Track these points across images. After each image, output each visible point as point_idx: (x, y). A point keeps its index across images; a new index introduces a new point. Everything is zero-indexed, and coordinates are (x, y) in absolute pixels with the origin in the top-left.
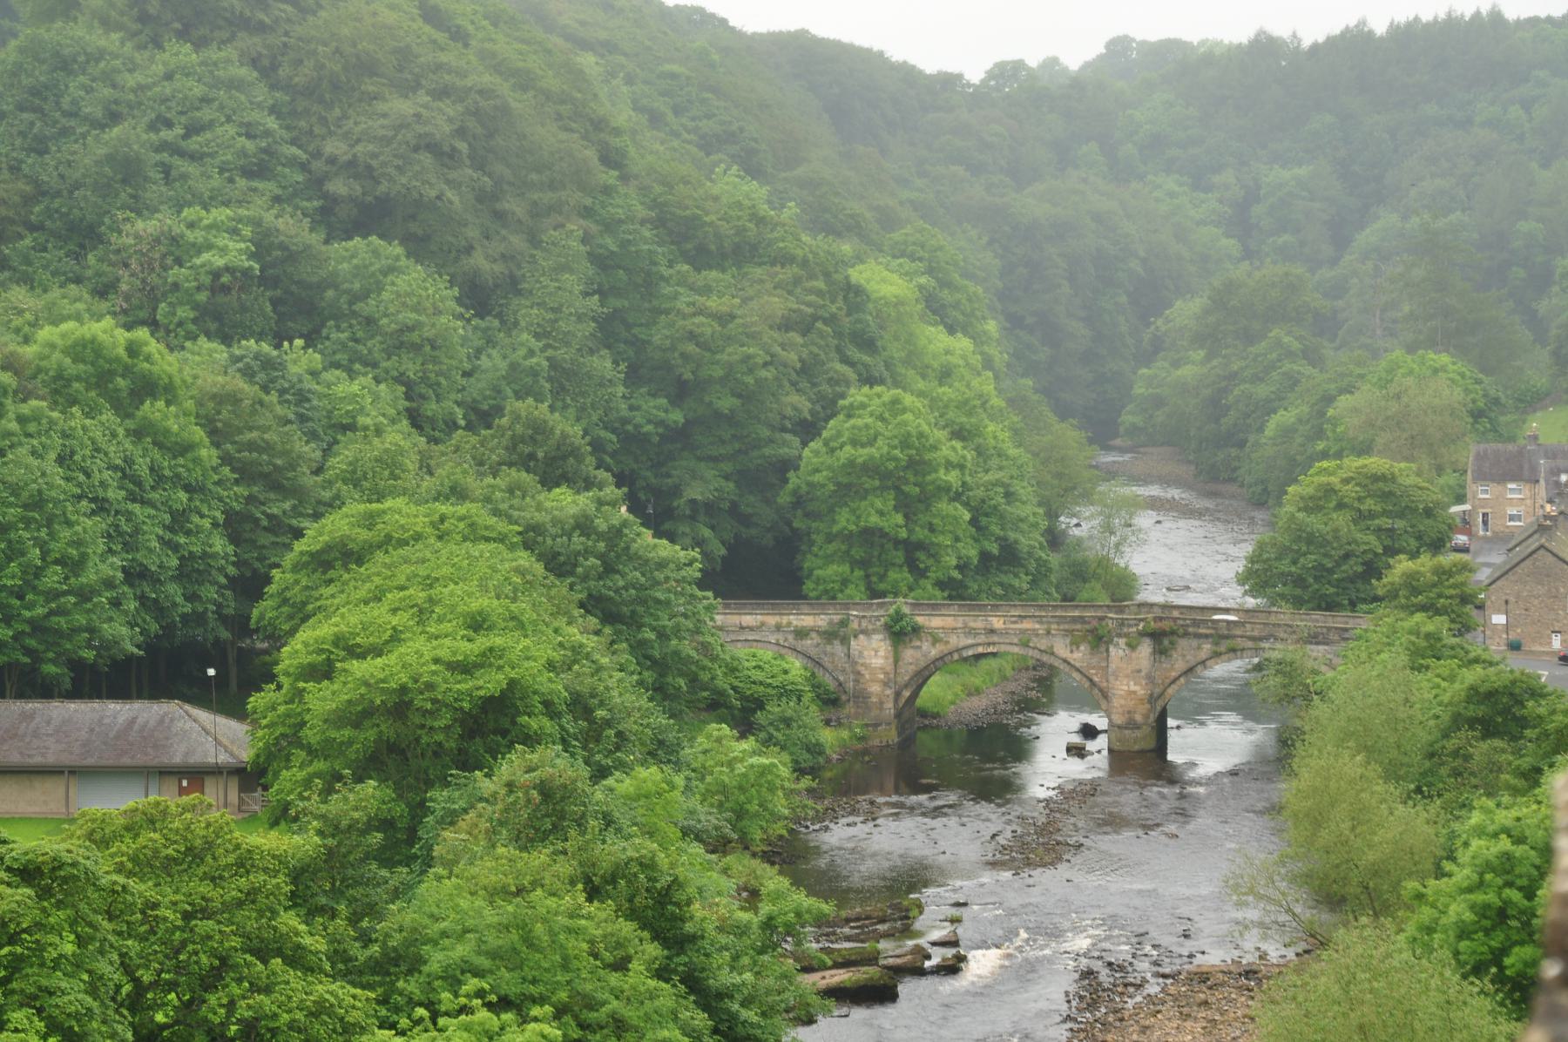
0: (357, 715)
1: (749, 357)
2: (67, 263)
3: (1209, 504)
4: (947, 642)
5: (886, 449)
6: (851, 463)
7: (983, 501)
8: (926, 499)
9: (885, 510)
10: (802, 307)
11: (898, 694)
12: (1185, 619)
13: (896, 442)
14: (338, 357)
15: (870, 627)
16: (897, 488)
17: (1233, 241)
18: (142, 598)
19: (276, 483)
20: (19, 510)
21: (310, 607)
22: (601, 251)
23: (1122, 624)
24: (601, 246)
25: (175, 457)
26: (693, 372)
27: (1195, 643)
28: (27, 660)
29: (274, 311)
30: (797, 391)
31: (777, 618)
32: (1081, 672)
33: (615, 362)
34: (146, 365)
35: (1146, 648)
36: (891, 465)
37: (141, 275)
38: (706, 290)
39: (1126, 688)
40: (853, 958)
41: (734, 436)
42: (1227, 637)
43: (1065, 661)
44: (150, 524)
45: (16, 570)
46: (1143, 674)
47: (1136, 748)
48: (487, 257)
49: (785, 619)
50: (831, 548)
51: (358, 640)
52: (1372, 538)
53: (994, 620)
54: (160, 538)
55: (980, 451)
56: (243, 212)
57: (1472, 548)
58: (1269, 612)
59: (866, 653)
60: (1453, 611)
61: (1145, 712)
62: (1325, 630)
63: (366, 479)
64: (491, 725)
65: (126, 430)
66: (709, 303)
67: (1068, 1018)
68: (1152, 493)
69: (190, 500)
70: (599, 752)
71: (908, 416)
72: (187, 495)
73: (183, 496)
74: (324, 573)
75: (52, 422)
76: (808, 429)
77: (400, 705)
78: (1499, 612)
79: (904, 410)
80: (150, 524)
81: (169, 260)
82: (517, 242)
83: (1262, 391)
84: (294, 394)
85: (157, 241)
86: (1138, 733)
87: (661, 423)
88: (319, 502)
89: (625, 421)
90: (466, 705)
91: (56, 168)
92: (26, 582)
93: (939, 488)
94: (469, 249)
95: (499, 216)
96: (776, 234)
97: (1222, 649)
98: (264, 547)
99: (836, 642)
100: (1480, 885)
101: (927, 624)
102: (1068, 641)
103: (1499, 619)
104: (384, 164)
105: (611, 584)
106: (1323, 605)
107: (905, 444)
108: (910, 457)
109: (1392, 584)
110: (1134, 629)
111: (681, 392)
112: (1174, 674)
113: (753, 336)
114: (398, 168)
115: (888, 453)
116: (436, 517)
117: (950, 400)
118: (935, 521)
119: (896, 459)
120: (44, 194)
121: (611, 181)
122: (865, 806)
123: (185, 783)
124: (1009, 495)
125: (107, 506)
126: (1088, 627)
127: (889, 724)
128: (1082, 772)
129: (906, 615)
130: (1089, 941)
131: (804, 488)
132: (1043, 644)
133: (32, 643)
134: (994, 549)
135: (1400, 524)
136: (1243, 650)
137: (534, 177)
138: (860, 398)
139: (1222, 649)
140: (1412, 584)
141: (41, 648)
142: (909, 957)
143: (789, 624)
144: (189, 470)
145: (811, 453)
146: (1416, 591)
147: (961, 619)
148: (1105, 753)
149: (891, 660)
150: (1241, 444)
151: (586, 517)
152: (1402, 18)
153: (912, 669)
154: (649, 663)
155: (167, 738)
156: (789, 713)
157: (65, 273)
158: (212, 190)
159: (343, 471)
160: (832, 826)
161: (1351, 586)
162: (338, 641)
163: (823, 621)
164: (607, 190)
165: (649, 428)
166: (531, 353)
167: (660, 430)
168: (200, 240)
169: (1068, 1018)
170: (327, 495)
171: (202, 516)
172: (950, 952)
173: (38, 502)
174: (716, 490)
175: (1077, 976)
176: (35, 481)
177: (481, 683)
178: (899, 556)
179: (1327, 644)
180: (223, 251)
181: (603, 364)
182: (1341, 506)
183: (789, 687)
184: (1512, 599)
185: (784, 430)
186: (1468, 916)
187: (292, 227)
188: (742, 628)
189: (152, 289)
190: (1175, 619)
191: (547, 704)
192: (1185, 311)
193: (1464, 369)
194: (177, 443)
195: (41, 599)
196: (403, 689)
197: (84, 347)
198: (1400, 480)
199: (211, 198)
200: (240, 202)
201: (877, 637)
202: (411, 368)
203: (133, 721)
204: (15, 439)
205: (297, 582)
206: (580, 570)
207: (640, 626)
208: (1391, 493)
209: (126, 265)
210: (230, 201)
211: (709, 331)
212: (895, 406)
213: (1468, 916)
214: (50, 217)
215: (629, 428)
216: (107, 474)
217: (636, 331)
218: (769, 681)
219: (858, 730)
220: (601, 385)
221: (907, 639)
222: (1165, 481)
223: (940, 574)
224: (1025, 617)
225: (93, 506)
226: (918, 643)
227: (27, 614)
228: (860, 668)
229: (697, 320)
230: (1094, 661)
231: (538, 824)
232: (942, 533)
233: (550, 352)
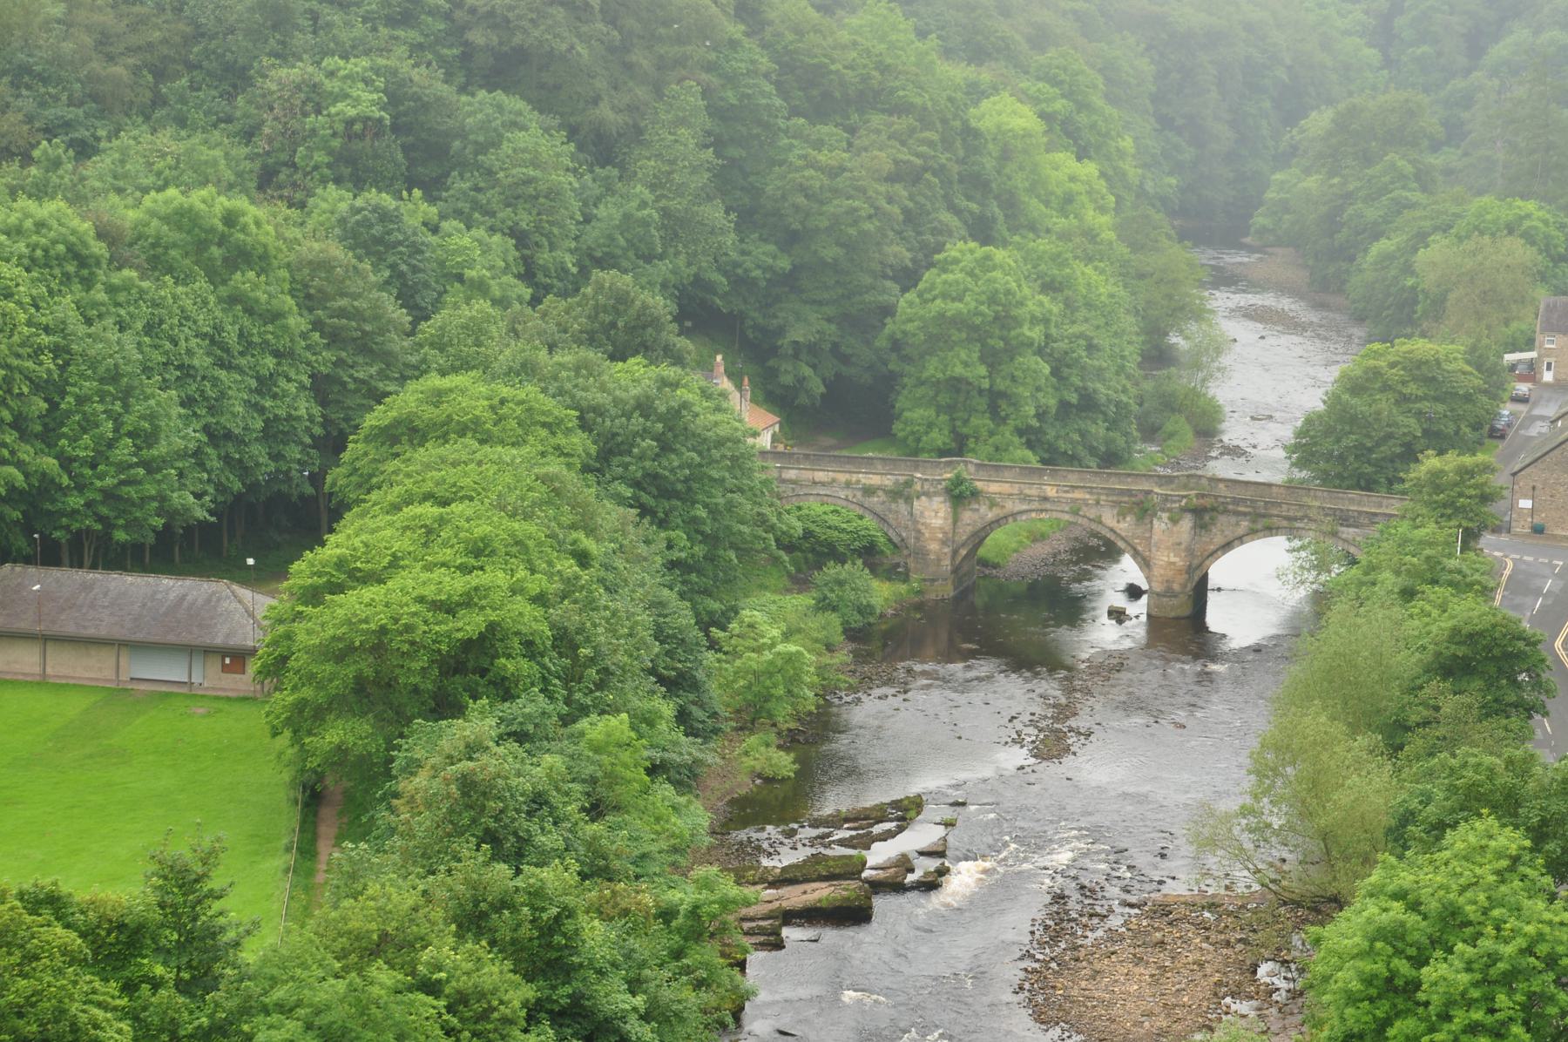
0: (340, 652)
1: (856, 210)
2: (219, 103)
3: (1313, 317)
4: (1003, 507)
5: (973, 304)
6: (941, 315)
7: (1066, 353)
8: (1012, 351)
10: (912, 158)
11: (955, 552)
13: (984, 297)
14: (460, 205)
15: (932, 490)
17: (1373, 51)
18: (227, 459)
19: (366, 347)
20: (95, 384)
21: (374, 480)
22: (722, 104)
23: (1166, 500)
24: (722, 99)
25: (265, 324)
27: (1233, 519)
28: (99, 527)
29: (406, 156)
30: (902, 239)
31: (847, 476)
32: (1126, 541)
33: (727, 212)
34: (241, 236)
35: (1187, 523)
36: (978, 320)
37: (283, 120)
38: (818, 145)
40: (837, 871)
41: (837, 282)
42: (1264, 516)
43: (1112, 530)
44: (236, 390)
45: (89, 442)
46: (1183, 547)
47: (1173, 614)
48: (613, 108)
49: (854, 478)
50: (920, 391)
51: (358, 564)
52: (1412, 421)
53: (1048, 488)
54: (247, 403)
55: (1068, 304)
56: (381, 61)
57: (1532, 400)
59: (926, 513)
60: (1472, 510)
63: (452, 345)
64: (471, 665)
65: (218, 297)
66: (821, 157)
67: (1029, 955)
68: (1267, 303)
69: (279, 364)
70: (580, 690)
71: (997, 274)
72: (274, 361)
73: (270, 362)
74: (392, 446)
75: (142, 292)
76: (908, 278)
77: (379, 645)
78: (1525, 497)
79: (994, 268)
80: (236, 390)
81: (309, 108)
82: (642, 93)
83: (1372, 214)
84: (407, 246)
85: (298, 88)
86: (1175, 601)
87: (771, 268)
88: (406, 365)
89: (736, 265)
90: (444, 648)
91: (213, 11)
92: (98, 452)
93: (1023, 344)
94: (596, 101)
95: (629, 67)
96: (897, 83)
97: (1259, 526)
98: (349, 408)
99: (901, 501)
100: (1368, 953)
101: (985, 488)
102: (1115, 512)
103: (1526, 504)
104: (520, 17)
105: (666, 464)
106: (1363, 483)
108: (997, 312)
109: (1419, 479)
111: (790, 239)
112: (1212, 547)
113: (863, 191)
114: (532, 20)
116: (496, 401)
117: (1045, 252)
118: (1016, 373)
120: (202, 35)
121: (738, 36)
122: (901, 674)
123: (227, 661)
124: (1091, 348)
125: (192, 372)
128: (1115, 642)
129: (965, 480)
130: (1070, 855)
131: (899, 336)
132: (1092, 513)
133: (104, 510)
134: (1073, 398)
135: (1440, 408)
136: (1278, 528)
137: (662, 31)
138: (954, 253)
139: (1259, 526)
140: (1435, 482)
141: (112, 514)
142: (892, 870)
143: (858, 482)
144: (277, 337)
145: (907, 303)
146: (1438, 489)
148: (1144, 618)
149: (950, 521)
150: (1352, 259)
151: (648, 397)
153: (969, 529)
154: (700, 538)
155: (212, 618)
156: (843, 576)
157: (216, 113)
158: (353, 40)
159: (432, 335)
160: (864, 698)
161: (1390, 465)
162: (340, 564)
163: (888, 481)
164: (733, 44)
165: (757, 273)
166: (643, 205)
167: (768, 276)
168: (336, 90)
169: (1029, 955)
170: (413, 359)
171: (289, 380)
172: (932, 864)
173: (114, 377)
174: (818, 332)
175: (1048, 899)
176: (111, 356)
177: (460, 624)
178: (982, 403)
179: (1357, 527)
180: (357, 100)
181: (715, 213)
183: (863, 533)
184: (1539, 486)
185: (885, 277)
186: (1355, 985)
187: (427, 80)
188: (815, 483)
189: (293, 133)
191: (528, 644)
192: (1319, 121)
193: (1548, 216)
194: (268, 310)
195: (112, 470)
196: (383, 630)
197: (182, 215)
198: (1445, 366)
199: (353, 47)
200: (382, 50)
201: (938, 499)
202: (525, 220)
203: (183, 598)
204: (103, 309)
205: (366, 454)
206: (636, 450)
207: (694, 503)
208: (1434, 379)
209: (272, 109)
210: (370, 51)
211: (818, 184)
212: (986, 264)
213: (1355, 985)
214: (207, 57)
215: (740, 271)
216: (194, 342)
217: (752, 179)
218: (844, 526)
219: (915, 585)
220: (712, 232)
221: (966, 502)
222: (1282, 289)
224: (1077, 487)
225: (178, 373)
227: (98, 484)
228: (920, 527)
229: (807, 173)
230: (1139, 531)
231: (455, 818)
232: (1023, 384)
233: (663, 203)
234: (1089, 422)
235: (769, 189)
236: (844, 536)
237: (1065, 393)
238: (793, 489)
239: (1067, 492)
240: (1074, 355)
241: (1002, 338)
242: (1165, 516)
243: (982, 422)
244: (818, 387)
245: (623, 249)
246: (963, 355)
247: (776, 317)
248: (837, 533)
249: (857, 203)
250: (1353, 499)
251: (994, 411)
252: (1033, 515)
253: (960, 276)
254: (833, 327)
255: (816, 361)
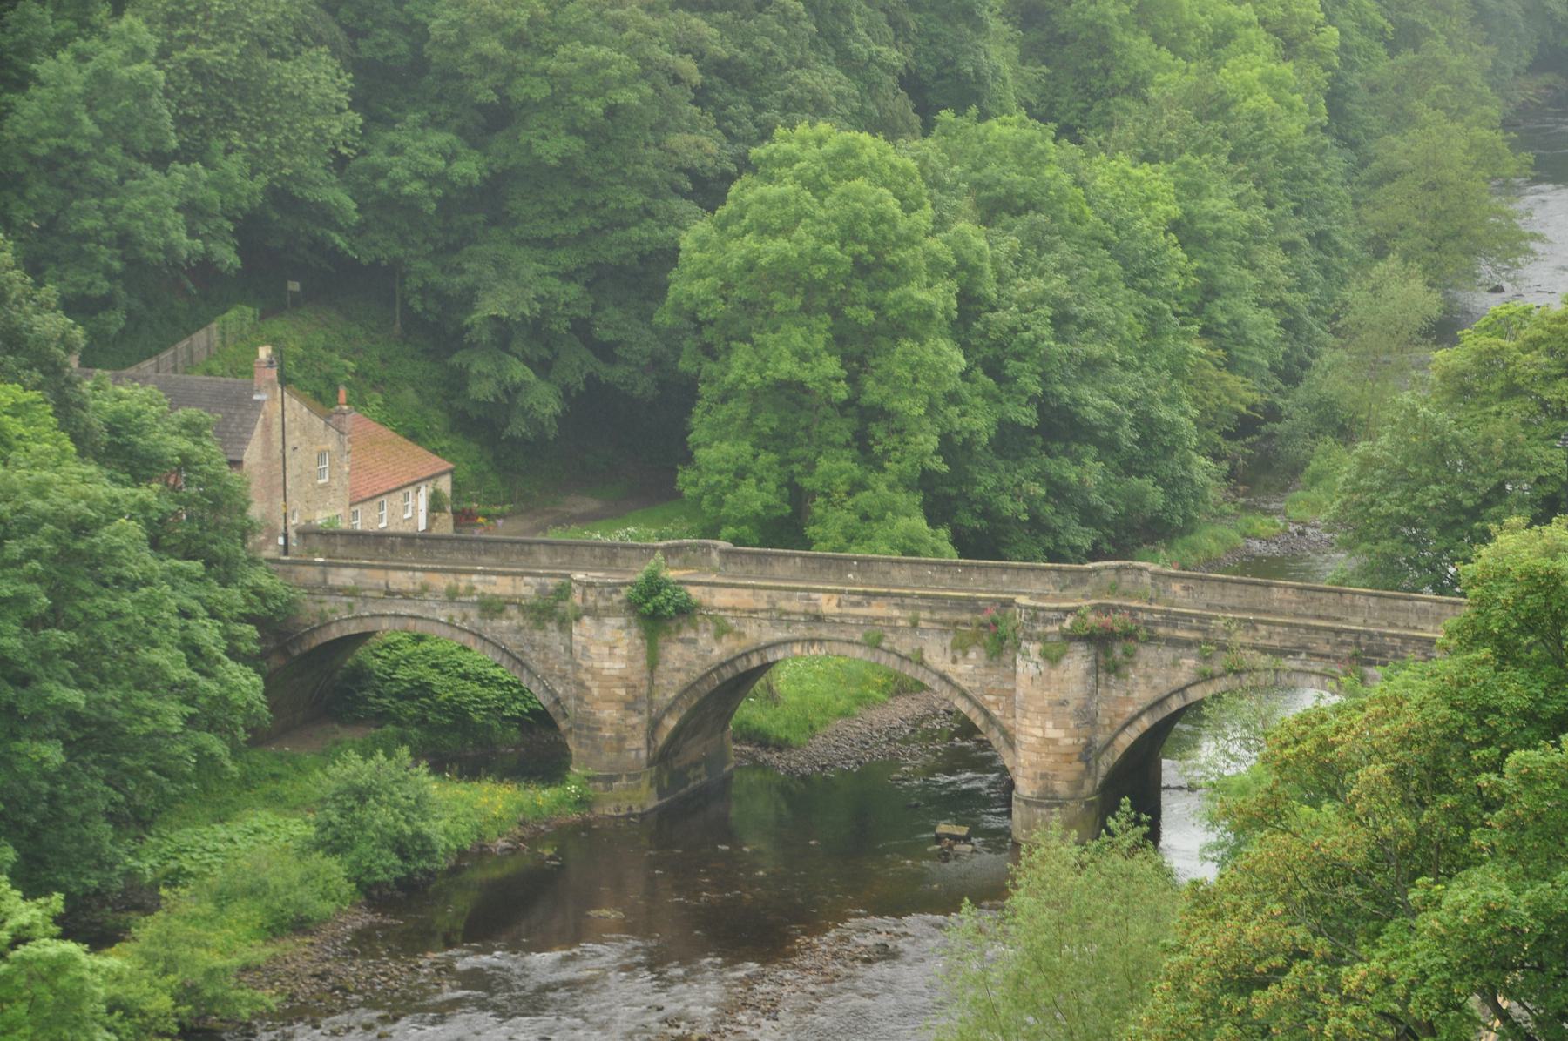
4: (741, 635)
5: (810, 242)
7: (1014, 330)
9: (810, 350)
11: (655, 724)
12: (1152, 612)
15: (601, 604)
16: (836, 313)
23: (1035, 618)
26: (496, 89)
27: (1168, 654)
32: (970, 699)
35: (1077, 662)
36: (820, 273)
39: (1039, 733)
43: (943, 677)
46: (1070, 708)
49: (463, 582)
53: (822, 598)
58: (1341, 593)
59: (593, 650)
61: (1072, 776)
62: (1398, 642)
99: (551, 626)
101: (706, 600)
102: (948, 642)
107: (849, 234)
108: (857, 259)
110: (1056, 628)
112: (1131, 709)
115: (816, 250)
119: (829, 261)
126: (982, 617)
127: (637, 776)
129: (667, 583)
132: (905, 645)
134: (1027, 416)
143: (471, 590)
147: (764, 593)
149: (641, 663)
163: (526, 588)
166: (138, 54)
174: (540, 299)
178: (842, 430)
182: (1512, 391)
188: (390, 593)
190: (1133, 611)
201: (613, 622)
215: (383, 184)
223: (906, 465)
224: (876, 595)
226: (691, 634)
230: (993, 679)
234: (1066, 461)
235: (435, 25)
236: (491, 693)
237: (1009, 406)
238: (350, 606)
239: (857, 604)
240: (1028, 335)
241: (872, 305)
242: (1034, 648)
243: (837, 466)
244: (545, 401)
245: (91, 138)
246: (798, 339)
247: (462, 272)
248: (477, 688)
249: (602, 53)
250: (1426, 611)
251: (862, 443)
252: (797, 649)
253: (789, 188)
254: (574, 290)
255: (545, 353)
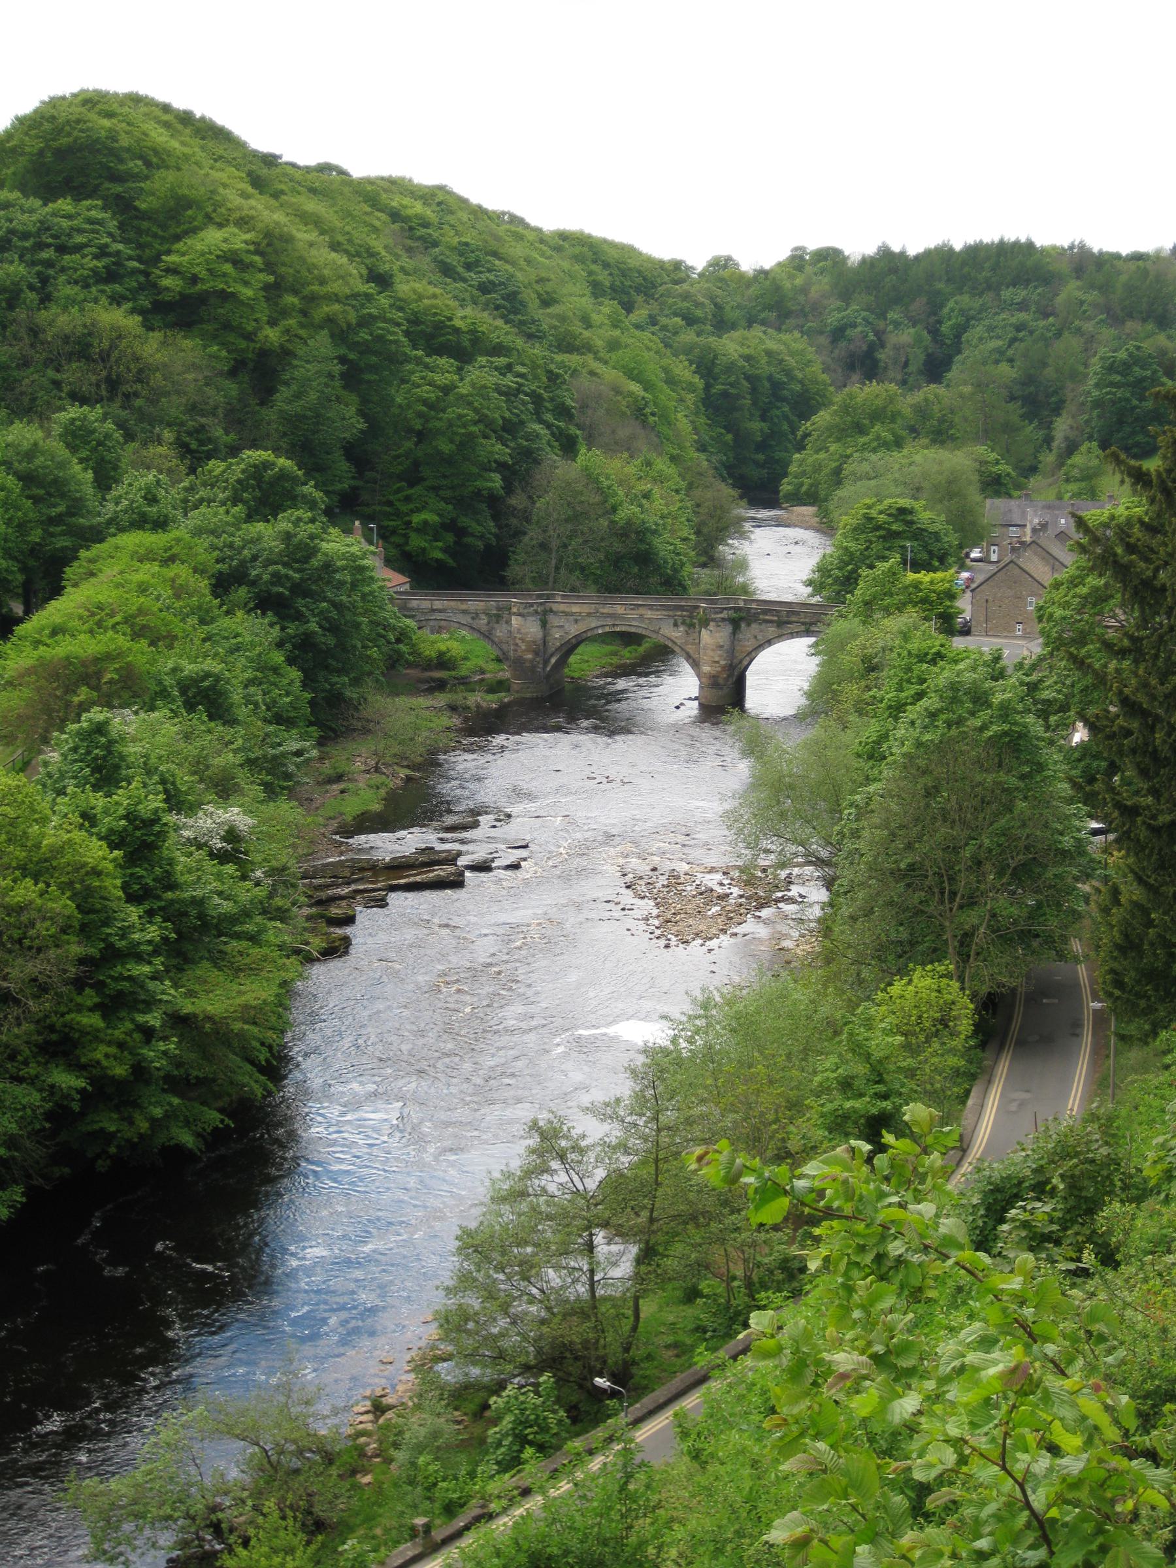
152: (971, 241)
188: (433, 610)
254: (450, 507)
